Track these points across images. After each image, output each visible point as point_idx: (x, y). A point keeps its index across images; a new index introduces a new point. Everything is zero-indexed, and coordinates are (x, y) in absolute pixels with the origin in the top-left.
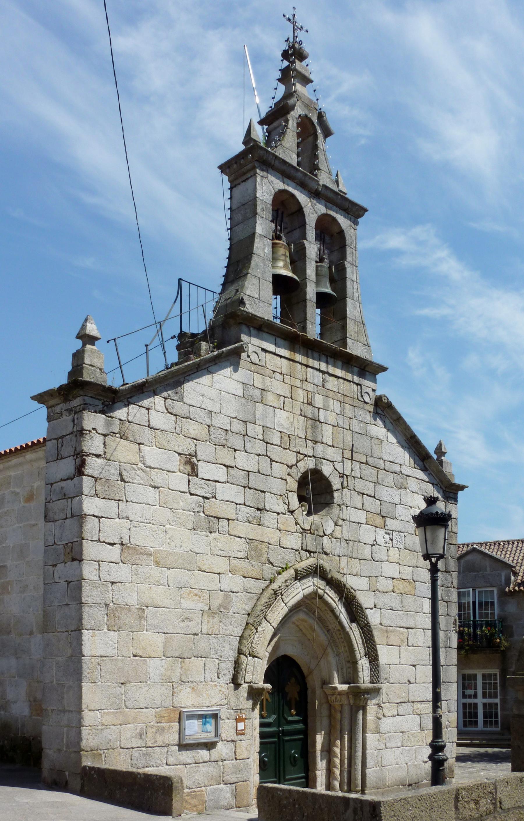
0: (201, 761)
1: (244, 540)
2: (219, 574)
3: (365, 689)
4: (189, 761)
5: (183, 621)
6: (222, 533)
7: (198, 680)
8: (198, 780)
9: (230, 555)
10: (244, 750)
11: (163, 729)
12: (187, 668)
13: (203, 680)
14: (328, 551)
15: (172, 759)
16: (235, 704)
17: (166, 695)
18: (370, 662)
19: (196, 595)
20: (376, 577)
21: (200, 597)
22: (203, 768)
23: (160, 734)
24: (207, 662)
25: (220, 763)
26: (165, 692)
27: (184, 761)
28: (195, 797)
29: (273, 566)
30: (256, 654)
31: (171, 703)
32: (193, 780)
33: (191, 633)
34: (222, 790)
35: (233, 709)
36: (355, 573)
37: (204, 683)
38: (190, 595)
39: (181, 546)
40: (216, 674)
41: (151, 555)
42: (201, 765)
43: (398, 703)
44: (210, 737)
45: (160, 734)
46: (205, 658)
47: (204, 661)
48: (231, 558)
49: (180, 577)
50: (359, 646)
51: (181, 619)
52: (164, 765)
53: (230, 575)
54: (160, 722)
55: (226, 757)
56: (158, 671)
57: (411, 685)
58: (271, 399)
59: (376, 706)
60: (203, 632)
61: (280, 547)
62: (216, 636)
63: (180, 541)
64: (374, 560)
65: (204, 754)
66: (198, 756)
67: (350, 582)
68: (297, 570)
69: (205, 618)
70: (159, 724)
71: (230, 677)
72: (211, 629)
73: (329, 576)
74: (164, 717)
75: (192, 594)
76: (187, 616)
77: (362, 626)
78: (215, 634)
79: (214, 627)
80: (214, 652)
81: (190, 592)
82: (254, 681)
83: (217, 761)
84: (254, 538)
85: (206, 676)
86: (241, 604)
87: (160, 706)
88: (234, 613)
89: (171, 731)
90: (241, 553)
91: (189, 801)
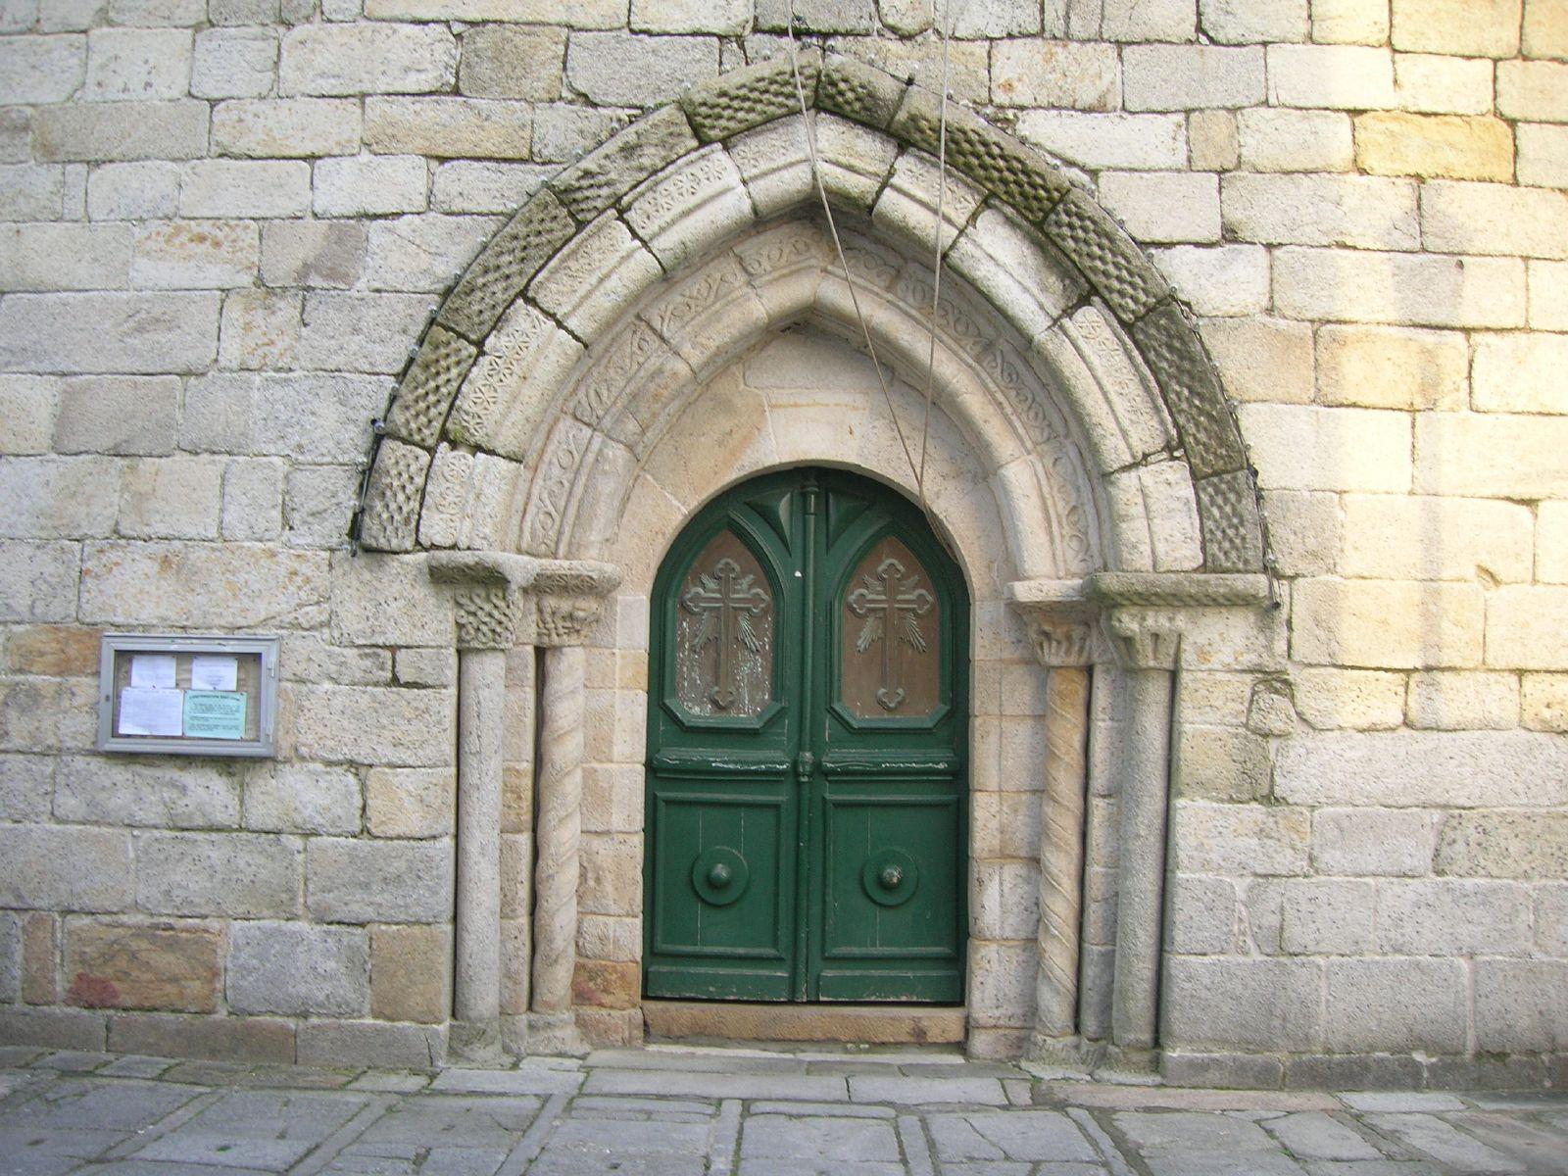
0: (200, 821)
1: (442, 28)
2: (311, 158)
3: (802, 196)
4: (151, 813)
5: (140, 329)
6: (334, 17)
7: (192, 532)
8: (186, 888)
9: (366, 87)
10: (409, 803)
11: (35, 695)
12: (145, 488)
13: (213, 533)
14: (908, 24)
15: (73, 802)
16: (364, 625)
17: (53, 580)
18: (1196, 476)
19: (202, 239)
20: (1234, 110)
21: (217, 244)
22: (214, 851)
23: (23, 711)
24: (234, 468)
25: (296, 842)
26: (50, 568)
27: (123, 814)
28: (172, 945)
29: (595, 105)
30: (479, 437)
31: (73, 607)
32: (164, 887)
33: (169, 368)
34: (299, 939)
35: (354, 645)
36: (1088, 97)
37: (219, 545)
38: (177, 242)
39: (148, 85)
40: (276, 514)
41: (26, 128)
42: (200, 836)
43: (1408, 672)
44: (229, 728)
45: (23, 711)
46: (230, 453)
47: (221, 468)
48: (368, 100)
49: (135, 184)
50: (1120, 405)
51: (131, 324)
52: (45, 817)
53: (365, 156)
54: (21, 671)
55: (319, 820)
56: (26, 502)
57: (1503, 589)
58: (1295, 554)
59: (1248, 678)
60: (223, 362)
61: (633, 32)
62: (283, 375)
63: (147, 68)
64: (1212, 40)
65: (210, 792)
66: (181, 803)
67: (1051, 135)
68: (691, 103)
69: (234, 311)
70: (20, 678)
71: (341, 523)
72: (260, 352)
73: (902, 116)
74: (42, 654)
75: (184, 238)
76: (157, 311)
77: (1127, 317)
78: (279, 370)
79: (272, 343)
80: (272, 434)
81: (178, 230)
82: (463, 542)
83: (278, 833)
84: (486, 16)
85: (227, 518)
86: (413, 260)
87: (27, 616)
88: (378, 291)
89: (66, 703)
90: (423, 76)
91: (143, 956)
